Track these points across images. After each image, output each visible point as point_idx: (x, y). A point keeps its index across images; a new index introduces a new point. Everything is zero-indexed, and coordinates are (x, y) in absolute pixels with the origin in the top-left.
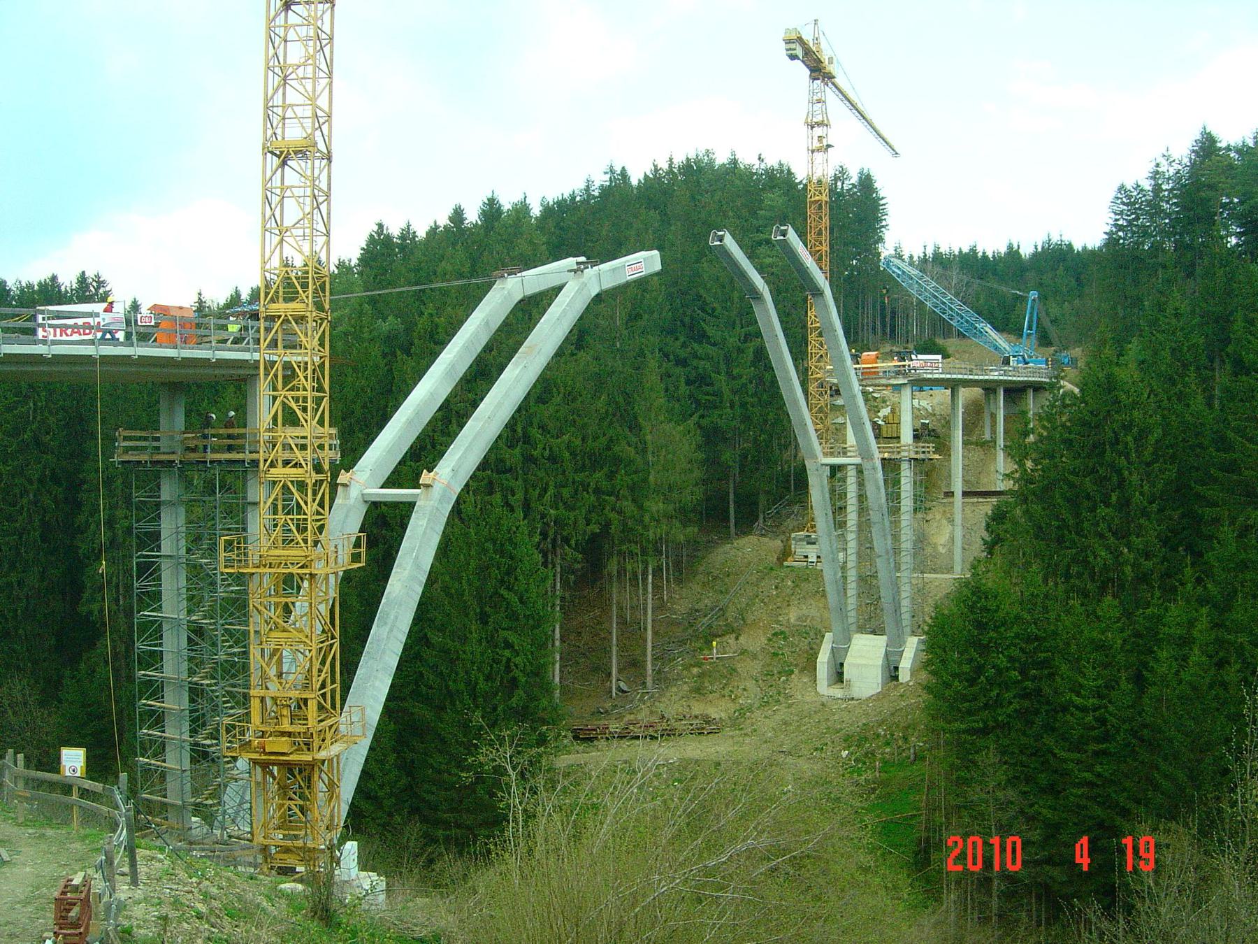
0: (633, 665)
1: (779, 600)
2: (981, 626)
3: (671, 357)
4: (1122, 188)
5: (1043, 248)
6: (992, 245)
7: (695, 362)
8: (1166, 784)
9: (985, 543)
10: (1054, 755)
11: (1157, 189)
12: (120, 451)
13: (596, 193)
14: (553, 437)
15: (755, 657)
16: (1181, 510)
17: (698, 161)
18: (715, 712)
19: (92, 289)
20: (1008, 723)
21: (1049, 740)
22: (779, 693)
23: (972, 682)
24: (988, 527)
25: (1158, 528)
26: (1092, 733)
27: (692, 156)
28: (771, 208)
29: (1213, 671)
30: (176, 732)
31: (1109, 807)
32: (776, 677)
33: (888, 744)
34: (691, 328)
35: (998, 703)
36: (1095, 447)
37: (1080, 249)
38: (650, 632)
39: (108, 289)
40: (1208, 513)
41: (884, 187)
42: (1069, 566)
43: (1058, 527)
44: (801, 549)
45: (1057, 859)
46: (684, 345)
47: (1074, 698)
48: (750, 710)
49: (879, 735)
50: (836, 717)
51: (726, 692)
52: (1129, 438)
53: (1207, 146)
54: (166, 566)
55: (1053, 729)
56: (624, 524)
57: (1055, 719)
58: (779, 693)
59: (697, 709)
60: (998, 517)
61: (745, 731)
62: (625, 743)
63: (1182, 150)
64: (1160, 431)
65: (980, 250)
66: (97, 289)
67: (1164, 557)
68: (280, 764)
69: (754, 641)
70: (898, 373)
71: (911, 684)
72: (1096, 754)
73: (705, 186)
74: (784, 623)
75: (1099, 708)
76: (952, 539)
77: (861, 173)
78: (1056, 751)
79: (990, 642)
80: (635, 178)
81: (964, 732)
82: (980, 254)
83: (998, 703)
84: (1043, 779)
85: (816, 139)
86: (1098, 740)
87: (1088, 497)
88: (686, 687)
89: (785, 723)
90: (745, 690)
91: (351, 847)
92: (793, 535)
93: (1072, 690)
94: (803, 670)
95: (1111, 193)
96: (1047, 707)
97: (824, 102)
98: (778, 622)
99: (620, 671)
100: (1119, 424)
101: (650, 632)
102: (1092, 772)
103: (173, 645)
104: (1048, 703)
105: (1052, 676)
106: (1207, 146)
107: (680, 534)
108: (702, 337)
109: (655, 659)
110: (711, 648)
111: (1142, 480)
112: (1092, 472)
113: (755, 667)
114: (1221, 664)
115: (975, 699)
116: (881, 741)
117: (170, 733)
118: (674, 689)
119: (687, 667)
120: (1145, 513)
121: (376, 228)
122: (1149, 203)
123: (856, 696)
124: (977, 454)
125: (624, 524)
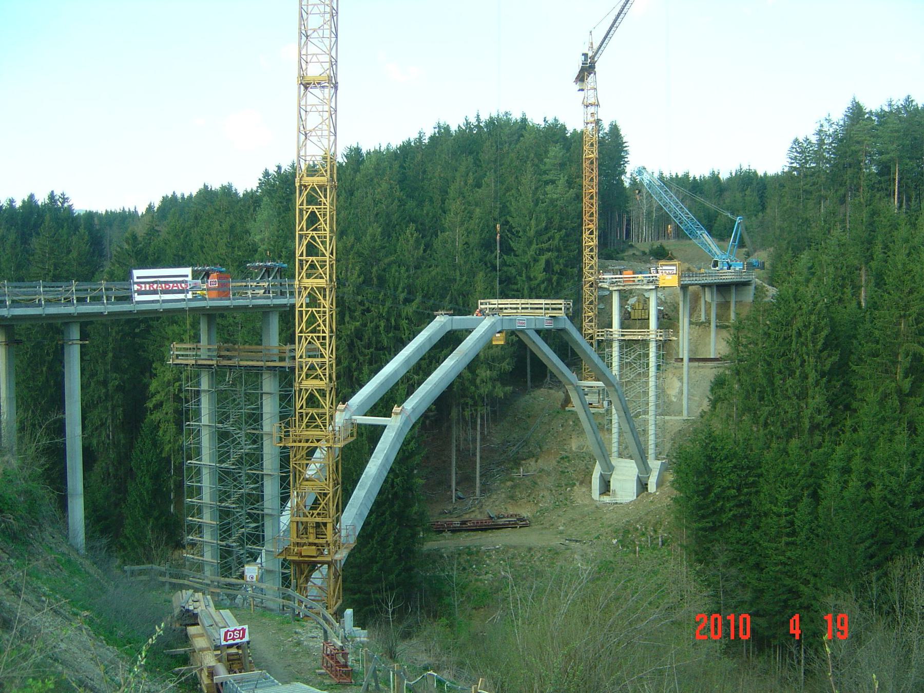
0: (466, 480)
3: (489, 265)
4: (796, 141)
6: (699, 171)
9: (710, 400)
10: (760, 545)
11: (821, 142)
12: (174, 357)
13: (426, 141)
14: (415, 325)
15: (549, 474)
17: (498, 119)
18: (525, 513)
19: (59, 203)
20: (729, 523)
24: (712, 390)
27: (494, 115)
29: (863, 490)
31: (796, 579)
32: (564, 487)
33: (644, 534)
35: (722, 509)
36: (785, 338)
37: (762, 175)
38: (478, 457)
39: (70, 204)
41: (627, 134)
42: (767, 418)
45: (761, 613)
49: (637, 529)
51: (531, 498)
53: (856, 113)
57: (760, 521)
60: (719, 383)
61: (545, 526)
62: (464, 534)
63: (839, 114)
65: (691, 176)
66: (63, 204)
68: (309, 563)
69: (548, 463)
70: (649, 282)
71: (657, 493)
72: (787, 544)
74: (568, 450)
75: (790, 514)
76: (681, 392)
77: (611, 125)
80: (454, 128)
82: (692, 178)
83: (722, 509)
84: (752, 560)
85: (589, 116)
86: (788, 535)
89: (573, 520)
91: (349, 612)
93: (771, 503)
94: (581, 483)
95: (789, 145)
96: (754, 513)
97: (596, 89)
98: (565, 450)
99: (457, 484)
101: (478, 457)
102: (785, 556)
103: (207, 482)
104: (755, 511)
105: (757, 492)
106: (856, 113)
107: (500, 391)
109: (481, 476)
111: (817, 362)
112: (783, 355)
115: (708, 508)
118: (495, 497)
119: (503, 482)
121: (276, 169)
124: (697, 330)
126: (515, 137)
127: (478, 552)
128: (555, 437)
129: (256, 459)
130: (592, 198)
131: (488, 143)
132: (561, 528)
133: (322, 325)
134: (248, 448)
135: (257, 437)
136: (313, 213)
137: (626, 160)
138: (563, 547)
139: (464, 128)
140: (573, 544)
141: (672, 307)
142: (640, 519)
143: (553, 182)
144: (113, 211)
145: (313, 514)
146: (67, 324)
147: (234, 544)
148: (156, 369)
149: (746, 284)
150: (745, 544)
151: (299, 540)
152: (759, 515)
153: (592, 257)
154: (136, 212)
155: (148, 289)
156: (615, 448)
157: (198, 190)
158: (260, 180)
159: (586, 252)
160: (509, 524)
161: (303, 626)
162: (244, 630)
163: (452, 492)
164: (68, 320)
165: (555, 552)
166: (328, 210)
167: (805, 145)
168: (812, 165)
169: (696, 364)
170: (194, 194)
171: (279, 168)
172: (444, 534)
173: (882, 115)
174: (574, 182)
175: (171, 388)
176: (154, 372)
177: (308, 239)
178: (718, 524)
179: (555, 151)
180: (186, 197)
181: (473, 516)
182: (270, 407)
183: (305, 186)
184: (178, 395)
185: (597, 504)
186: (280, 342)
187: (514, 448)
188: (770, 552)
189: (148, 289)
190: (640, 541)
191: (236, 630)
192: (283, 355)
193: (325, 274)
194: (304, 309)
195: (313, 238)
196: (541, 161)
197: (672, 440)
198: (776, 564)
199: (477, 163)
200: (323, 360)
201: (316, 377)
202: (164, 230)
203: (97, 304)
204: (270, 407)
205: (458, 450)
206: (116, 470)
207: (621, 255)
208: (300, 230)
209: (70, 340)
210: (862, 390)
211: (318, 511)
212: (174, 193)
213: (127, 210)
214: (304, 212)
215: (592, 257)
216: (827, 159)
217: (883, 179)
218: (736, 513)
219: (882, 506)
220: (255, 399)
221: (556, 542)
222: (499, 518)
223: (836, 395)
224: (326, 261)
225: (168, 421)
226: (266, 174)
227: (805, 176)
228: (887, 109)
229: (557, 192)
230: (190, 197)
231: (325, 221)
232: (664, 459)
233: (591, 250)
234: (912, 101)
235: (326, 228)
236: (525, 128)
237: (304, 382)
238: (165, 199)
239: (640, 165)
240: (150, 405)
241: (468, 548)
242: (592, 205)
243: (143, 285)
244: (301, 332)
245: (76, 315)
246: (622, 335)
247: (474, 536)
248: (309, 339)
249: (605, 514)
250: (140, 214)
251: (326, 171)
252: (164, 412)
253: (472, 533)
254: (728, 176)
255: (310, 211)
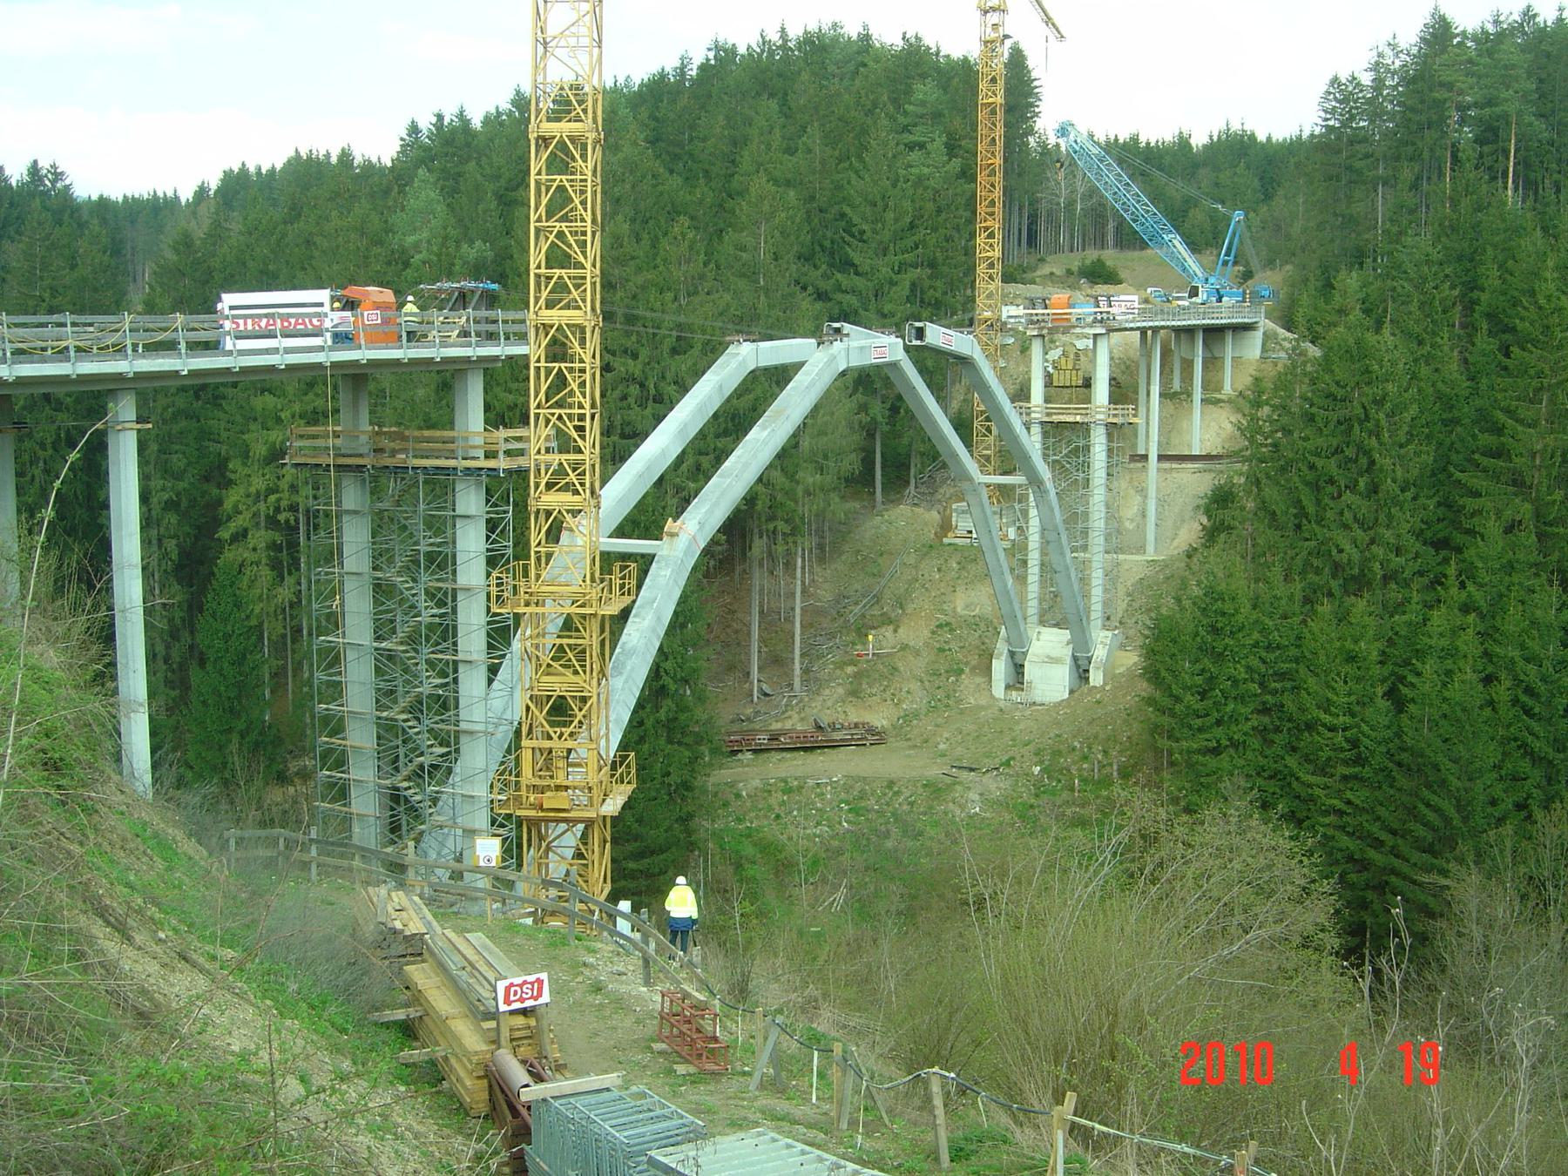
0: (776, 661)
1: (942, 584)
2: (1215, 630)
4: (1335, 81)
5: (1219, 137)
6: (1156, 131)
7: (839, 296)
8: (1431, 816)
10: (1297, 779)
11: (1378, 84)
13: (694, 73)
15: (917, 653)
16: (1436, 499)
17: (820, 35)
18: (879, 718)
19: (47, 182)
21: (1291, 761)
22: (948, 697)
23: (1203, 695)
25: (1412, 520)
26: (1341, 756)
27: (813, 27)
28: (923, 104)
30: (364, 774)
31: (1359, 838)
34: (832, 254)
35: (1234, 719)
38: (798, 625)
40: (1471, 504)
43: (1295, 516)
44: (963, 524)
46: (825, 276)
47: (1322, 716)
48: (916, 715)
49: (1074, 749)
50: (1022, 726)
52: (1382, 416)
53: (1439, 33)
54: (349, 585)
55: (1294, 749)
56: (773, 498)
58: (948, 697)
59: (854, 716)
60: (1221, 499)
62: (776, 756)
63: (1410, 36)
64: (1415, 406)
65: (1143, 139)
66: (54, 182)
67: (1417, 553)
69: (915, 632)
72: (1345, 778)
73: (832, 68)
78: (1301, 774)
79: (1225, 650)
81: (1199, 751)
82: (1143, 144)
85: (989, 30)
86: (1346, 763)
87: (1331, 481)
88: (840, 690)
90: (908, 692)
92: (954, 506)
100: (1370, 397)
101: (798, 625)
104: (1290, 720)
106: (1439, 33)
108: (847, 265)
109: (802, 655)
110: (865, 643)
113: (919, 665)
114: (1488, 680)
115: (1207, 715)
116: (1077, 755)
117: (355, 774)
118: (827, 692)
119: (840, 666)
120: (1396, 502)
121: (434, 120)
122: (1369, 102)
123: (1038, 700)
125: (773, 498)
126: (851, 66)
127: (800, 788)
128: (927, 590)
129: (446, 632)
130: (993, 173)
131: (805, 76)
132: (942, 746)
133: (578, 393)
134: (428, 613)
135: (446, 594)
136: (561, 189)
137: (1037, 110)
138: (948, 780)
139: (758, 50)
140: (964, 775)
141: (1123, 367)
142: (1080, 730)
143: (922, 146)
144: (137, 196)
145: (561, 735)
146: (112, 392)
147: (405, 784)
148: (235, 472)
149: (1248, 327)
150: (1271, 777)
151: (538, 782)
152: (1297, 728)
153: (991, 277)
154: (177, 198)
155: (250, 327)
156: (1033, 607)
157: (285, 160)
158: (402, 139)
159: (981, 269)
160: (852, 739)
161: (594, 952)
162: (540, 982)
163: (752, 683)
164: (115, 384)
165: (935, 790)
166: (589, 184)
167: (1350, 89)
168: (1362, 124)
169: (1167, 465)
170: (279, 166)
171: (440, 117)
172: (740, 756)
173: (1482, 38)
174: (959, 146)
175: (262, 506)
176: (232, 476)
177: (552, 237)
178: (1225, 742)
179: (925, 91)
180: (264, 171)
181: (788, 725)
182: (471, 543)
183: (544, 139)
184: (274, 517)
185: (1002, 704)
186: (486, 423)
187: (857, 609)
188: (1318, 791)
189: (250, 327)
190: (1080, 770)
191: (525, 982)
192: (493, 448)
193: (584, 301)
194: (542, 364)
195: (560, 235)
196: (898, 107)
197: (1129, 595)
198: (1326, 813)
199: (786, 111)
200: (579, 457)
201: (565, 488)
202: (236, 226)
203: (169, 357)
204: (471, 543)
205: (761, 612)
206: (168, 647)
207: (1029, 276)
208: (537, 221)
209: (118, 423)
210: (1473, 515)
211: (571, 729)
212: (243, 164)
213: (162, 195)
214: (543, 189)
215: (991, 277)
216: (1387, 113)
217: (1486, 149)
218: (1256, 724)
219: (1511, 716)
220: (442, 525)
221: (935, 771)
222: (834, 730)
223: (1426, 523)
224: (585, 278)
225: (258, 563)
226: (414, 129)
227: (1351, 143)
228: (1491, 28)
229: (931, 165)
230: (272, 171)
231: (584, 203)
232: (1116, 628)
233: (991, 266)
234: (1535, 15)
235: (587, 216)
236: (867, 51)
237: (544, 498)
238: (228, 176)
239: (1063, 118)
240: (224, 534)
241: (785, 781)
242: (993, 185)
243: (241, 322)
244: (538, 407)
245: (131, 375)
246: (1048, 415)
247: (791, 759)
248: (554, 419)
249: (1018, 723)
250: (183, 202)
251: (585, 111)
252: (251, 546)
253: (788, 755)
254: (1205, 140)
255: (555, 185)
